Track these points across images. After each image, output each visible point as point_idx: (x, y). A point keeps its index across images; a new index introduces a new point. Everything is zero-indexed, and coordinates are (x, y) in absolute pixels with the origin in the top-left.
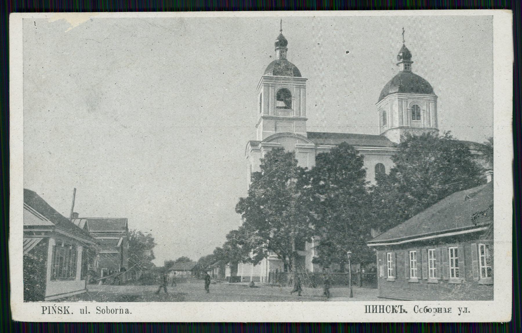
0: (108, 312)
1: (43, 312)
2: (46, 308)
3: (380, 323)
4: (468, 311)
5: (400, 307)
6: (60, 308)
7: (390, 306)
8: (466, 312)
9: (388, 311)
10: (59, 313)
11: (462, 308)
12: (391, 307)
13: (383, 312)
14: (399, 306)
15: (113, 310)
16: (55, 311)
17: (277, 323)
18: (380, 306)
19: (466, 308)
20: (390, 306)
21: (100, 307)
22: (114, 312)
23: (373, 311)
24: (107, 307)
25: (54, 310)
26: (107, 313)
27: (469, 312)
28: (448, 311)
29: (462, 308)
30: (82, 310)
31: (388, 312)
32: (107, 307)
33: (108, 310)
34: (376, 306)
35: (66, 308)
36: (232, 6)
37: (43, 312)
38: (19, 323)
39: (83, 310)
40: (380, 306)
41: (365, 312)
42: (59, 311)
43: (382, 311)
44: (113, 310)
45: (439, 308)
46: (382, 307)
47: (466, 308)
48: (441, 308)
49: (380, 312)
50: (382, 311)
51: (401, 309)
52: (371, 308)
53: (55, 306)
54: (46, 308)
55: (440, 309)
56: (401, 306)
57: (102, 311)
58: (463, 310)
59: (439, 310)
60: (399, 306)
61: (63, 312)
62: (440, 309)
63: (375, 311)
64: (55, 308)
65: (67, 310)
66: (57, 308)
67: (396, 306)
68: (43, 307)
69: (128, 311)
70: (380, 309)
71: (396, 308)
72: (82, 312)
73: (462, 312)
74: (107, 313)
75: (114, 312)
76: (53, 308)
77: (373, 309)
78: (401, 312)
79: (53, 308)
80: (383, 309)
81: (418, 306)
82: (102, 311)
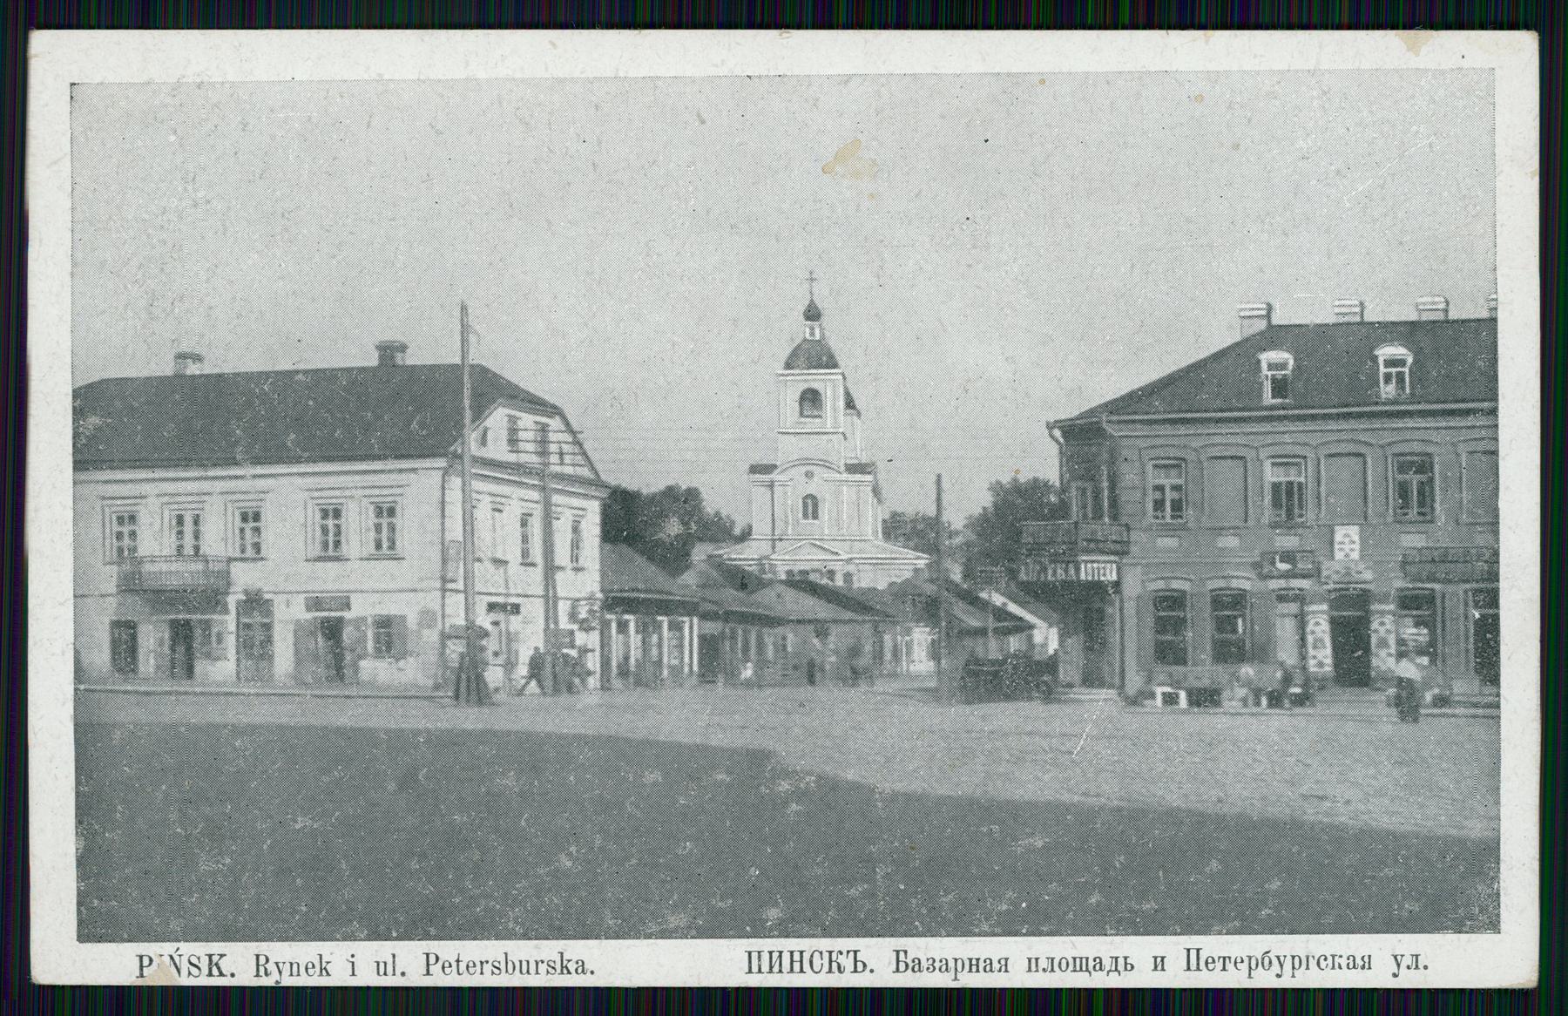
0: (510, 970)
1: (428, 970)
2: (151, 960)
3: (687, 28)
4: (1421, 966)
5: (852, 954)
6: (194, 960)
7: (821, 953)
8: (1417, 967)
9: (817, 968)
10: (190, 973)
11: (1402, 956)
12: (826, 955)
13: (802, 971)
14: (848, 952)
15: (1064, 961)
16: (176, 967)
17: (550, 28)
18: (792, 953)
19: (1417, 956)
20: (821, 953)
21: (199, 958)
22: (1060, 963)
23: (771, 967)
24: (506, 954)
25: (175, 964)
26: (507, 971)
27: (592, 972)
28: (1005, 965)
29: (1402, 956)
30: (382, 966)
31: (816, 970)
32: (506, 954)
33: (510, 964)
34: (781, 952)
35: (834, 958)
36: (560, 18)
37: (428, 970)
38: (1527, 27)
39: (528, 962)
40: (792, 953)
41: (1153, 967)
42: (191, 967)
43: (797, 967)
44: (1064, 961)
45: (971, 960)
46: (797, 957)
47: (1417, 956)
48: (978, 960)
49: (792, 970)
50: (797, 967)
51: (856, 961)
52: (766, 957)
53: (179, 953)
54: (151, 960)
55: (974, 962)
56: (855, 952)
57: (1263, 963)
58: (1407, 961)
59: (971, 965)
60: (848, 952)
61: (559, 971)
62: (974, 962)
63: (776, 969)
64: (177, 959)
65: (217, 964)
66: (185, 959)
67: (841, 953)
68: (141, 957)
69: (583, 965)
70: (792, 962)
71: (1340, 960)
72: (382, 972)
73: (1403, 965)
74: (507, 971)
75: (1060, 963)
76: (171, 957)
77: (771, 962)
78: (856, 971)
79: (171, 957)
80: (801, 962)
81: (906, 952)
82: (1263, 963)
